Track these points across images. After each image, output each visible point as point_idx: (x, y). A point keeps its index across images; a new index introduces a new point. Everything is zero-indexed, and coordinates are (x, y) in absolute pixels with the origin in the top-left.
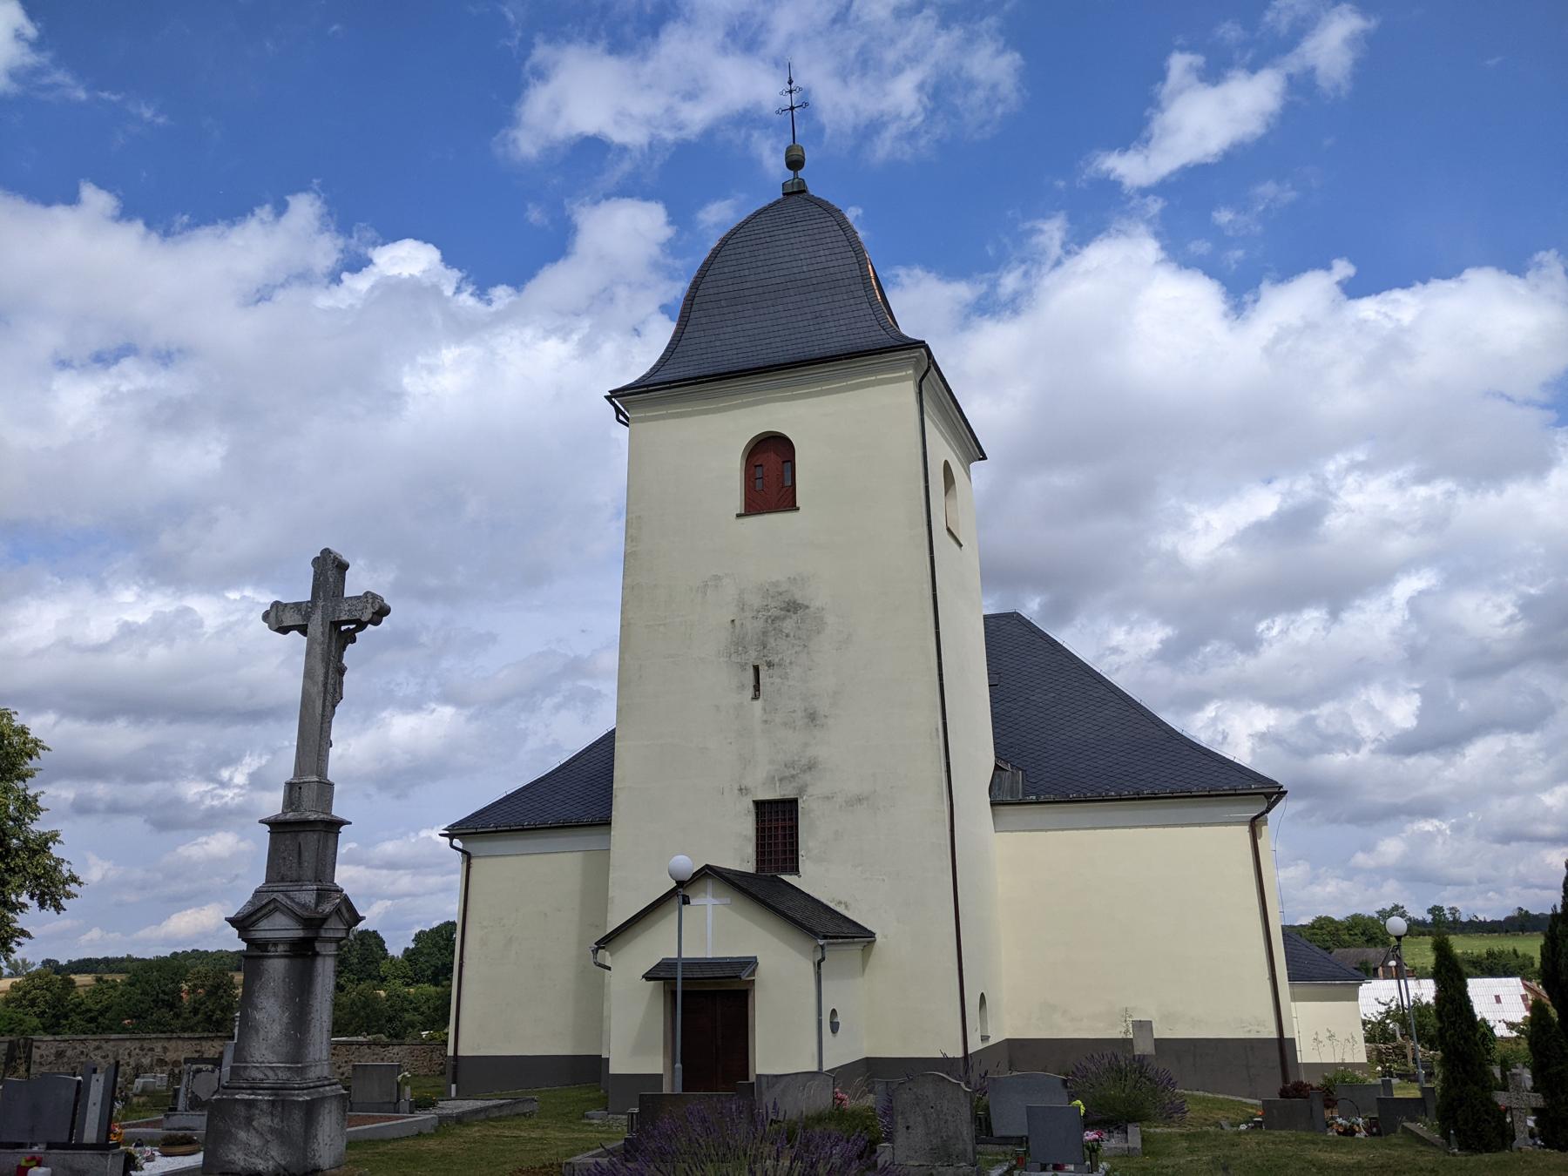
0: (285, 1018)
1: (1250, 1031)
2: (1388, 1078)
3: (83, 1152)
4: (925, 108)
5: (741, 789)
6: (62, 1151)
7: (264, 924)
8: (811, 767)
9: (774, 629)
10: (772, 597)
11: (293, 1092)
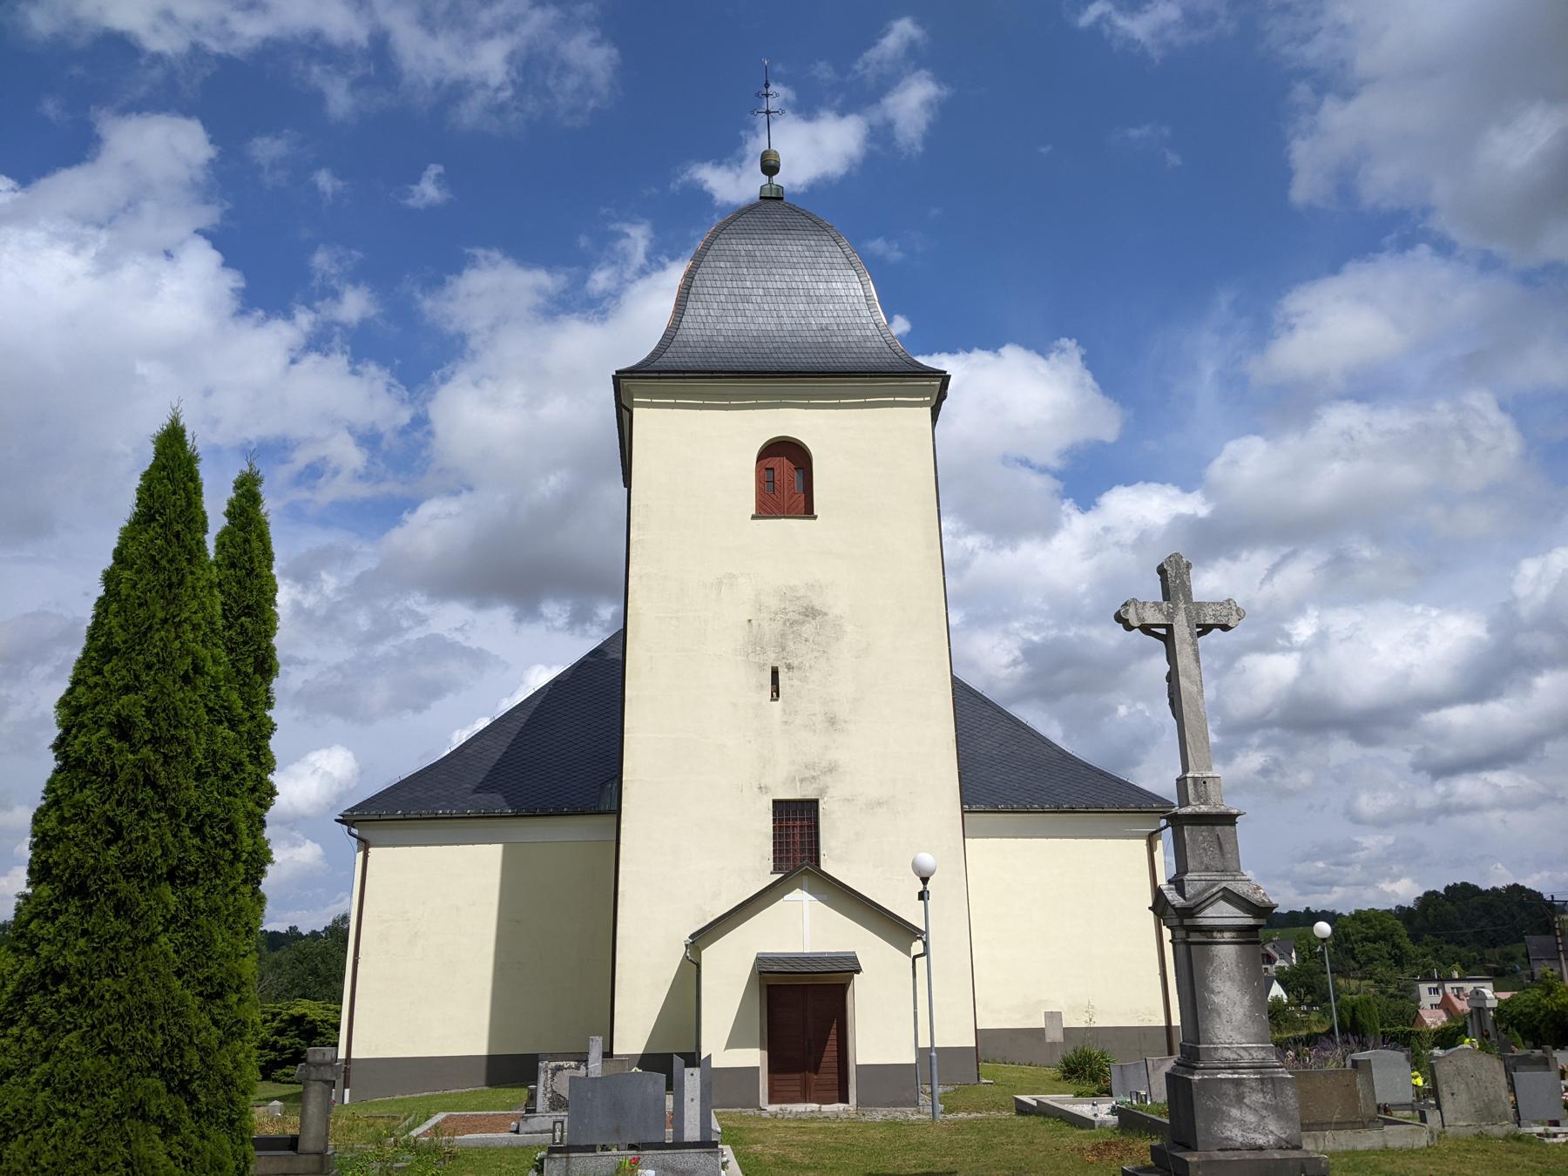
0: (1246, 1001)
1: (1143, 1020)
2: (934, 1054)
3: (686, 1151)
4: (513, 82)
5: (760, 788)
6: (660, 1152)
7: (1209, 912)
8: (831, 769)
9: (793, 632)
10: (790, 601)
11: (1276, 1070)
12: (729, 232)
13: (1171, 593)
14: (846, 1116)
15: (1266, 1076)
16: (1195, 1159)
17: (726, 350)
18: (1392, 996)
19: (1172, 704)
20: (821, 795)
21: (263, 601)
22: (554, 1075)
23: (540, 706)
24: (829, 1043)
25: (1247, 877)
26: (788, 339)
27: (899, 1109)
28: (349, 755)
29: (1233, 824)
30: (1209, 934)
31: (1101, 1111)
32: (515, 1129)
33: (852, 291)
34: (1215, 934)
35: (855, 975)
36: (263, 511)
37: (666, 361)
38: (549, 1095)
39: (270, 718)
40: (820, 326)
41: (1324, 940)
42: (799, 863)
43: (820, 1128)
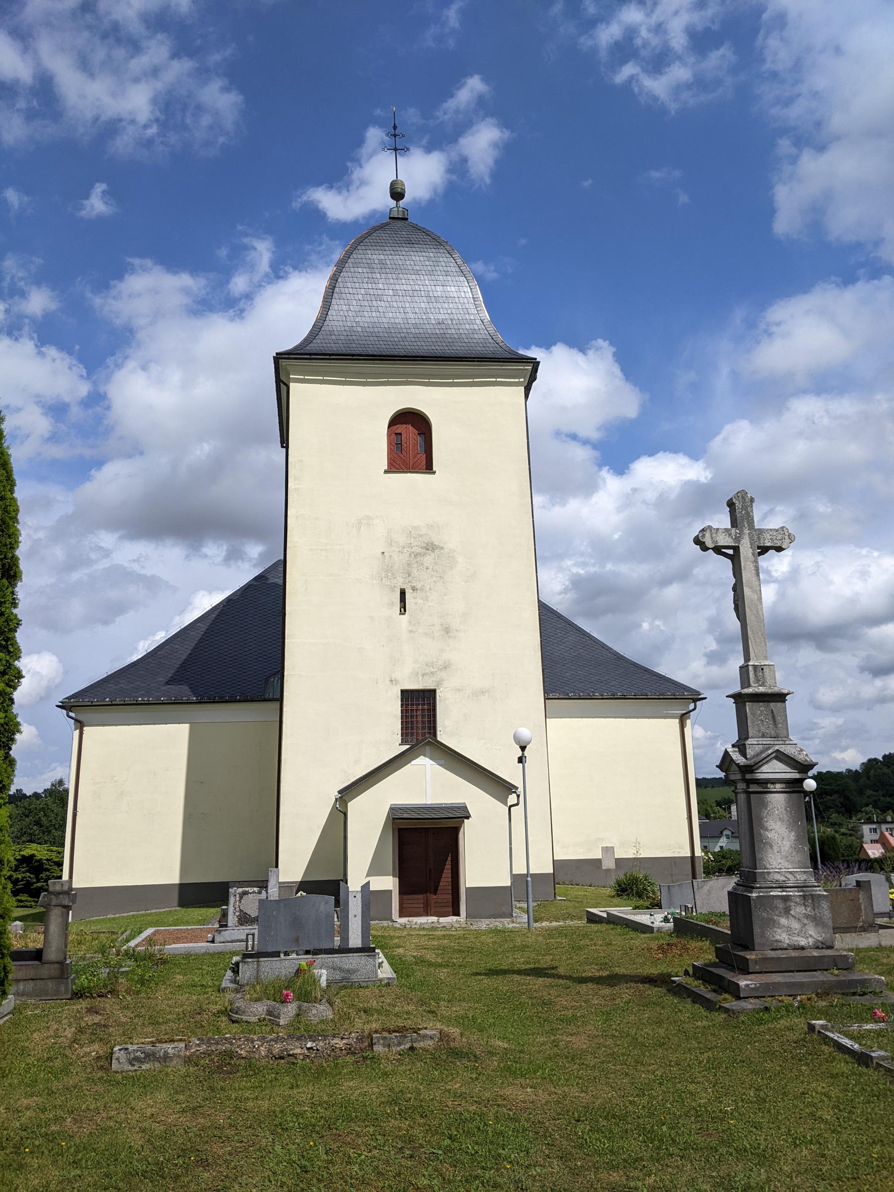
2: (529, 879)
3: (351, 955)
5: (391, 681)
6: (330, 956)
7: (765, 768)
8: (446, 667)
12: (365, 244)
13: (738, 521)
14: (459, 925)
15: (807, 893)
16: (753, 957)
17: (363, 338)
18: (844, 834)
19: (736, 609)
20: (438, 686)
21: (7, 519)
22: (241, 898)
23: (216, 618)
24: (445, 871)
25: (795, 742)
26: (413, 331)
27: (498, 920)
28: (54, 659)
29: (784, 701)
30: (764, 785)
31: (655, 919)
32: (211, 939)
33: (463, 293)
34: (769, 785)
35: (465, 820)
36: (5, 445)
37: (313, 347)
38: (238, 914)
39: (16, 615)
40: (437, 321)
41: (811, 792)
42: (420, 738)
43: (444, 936)
